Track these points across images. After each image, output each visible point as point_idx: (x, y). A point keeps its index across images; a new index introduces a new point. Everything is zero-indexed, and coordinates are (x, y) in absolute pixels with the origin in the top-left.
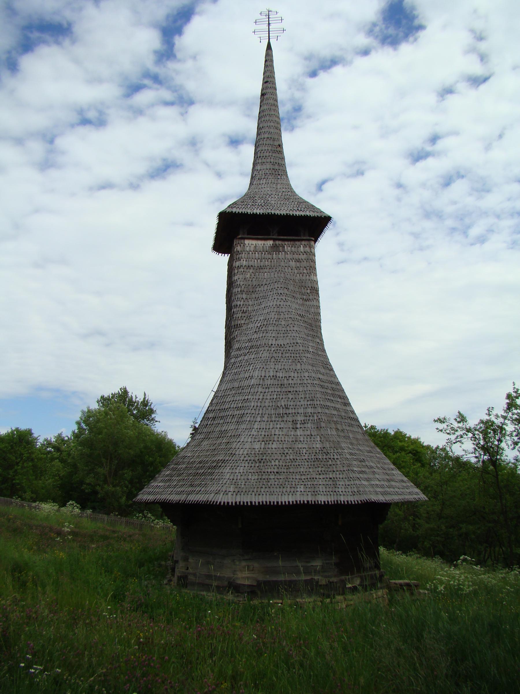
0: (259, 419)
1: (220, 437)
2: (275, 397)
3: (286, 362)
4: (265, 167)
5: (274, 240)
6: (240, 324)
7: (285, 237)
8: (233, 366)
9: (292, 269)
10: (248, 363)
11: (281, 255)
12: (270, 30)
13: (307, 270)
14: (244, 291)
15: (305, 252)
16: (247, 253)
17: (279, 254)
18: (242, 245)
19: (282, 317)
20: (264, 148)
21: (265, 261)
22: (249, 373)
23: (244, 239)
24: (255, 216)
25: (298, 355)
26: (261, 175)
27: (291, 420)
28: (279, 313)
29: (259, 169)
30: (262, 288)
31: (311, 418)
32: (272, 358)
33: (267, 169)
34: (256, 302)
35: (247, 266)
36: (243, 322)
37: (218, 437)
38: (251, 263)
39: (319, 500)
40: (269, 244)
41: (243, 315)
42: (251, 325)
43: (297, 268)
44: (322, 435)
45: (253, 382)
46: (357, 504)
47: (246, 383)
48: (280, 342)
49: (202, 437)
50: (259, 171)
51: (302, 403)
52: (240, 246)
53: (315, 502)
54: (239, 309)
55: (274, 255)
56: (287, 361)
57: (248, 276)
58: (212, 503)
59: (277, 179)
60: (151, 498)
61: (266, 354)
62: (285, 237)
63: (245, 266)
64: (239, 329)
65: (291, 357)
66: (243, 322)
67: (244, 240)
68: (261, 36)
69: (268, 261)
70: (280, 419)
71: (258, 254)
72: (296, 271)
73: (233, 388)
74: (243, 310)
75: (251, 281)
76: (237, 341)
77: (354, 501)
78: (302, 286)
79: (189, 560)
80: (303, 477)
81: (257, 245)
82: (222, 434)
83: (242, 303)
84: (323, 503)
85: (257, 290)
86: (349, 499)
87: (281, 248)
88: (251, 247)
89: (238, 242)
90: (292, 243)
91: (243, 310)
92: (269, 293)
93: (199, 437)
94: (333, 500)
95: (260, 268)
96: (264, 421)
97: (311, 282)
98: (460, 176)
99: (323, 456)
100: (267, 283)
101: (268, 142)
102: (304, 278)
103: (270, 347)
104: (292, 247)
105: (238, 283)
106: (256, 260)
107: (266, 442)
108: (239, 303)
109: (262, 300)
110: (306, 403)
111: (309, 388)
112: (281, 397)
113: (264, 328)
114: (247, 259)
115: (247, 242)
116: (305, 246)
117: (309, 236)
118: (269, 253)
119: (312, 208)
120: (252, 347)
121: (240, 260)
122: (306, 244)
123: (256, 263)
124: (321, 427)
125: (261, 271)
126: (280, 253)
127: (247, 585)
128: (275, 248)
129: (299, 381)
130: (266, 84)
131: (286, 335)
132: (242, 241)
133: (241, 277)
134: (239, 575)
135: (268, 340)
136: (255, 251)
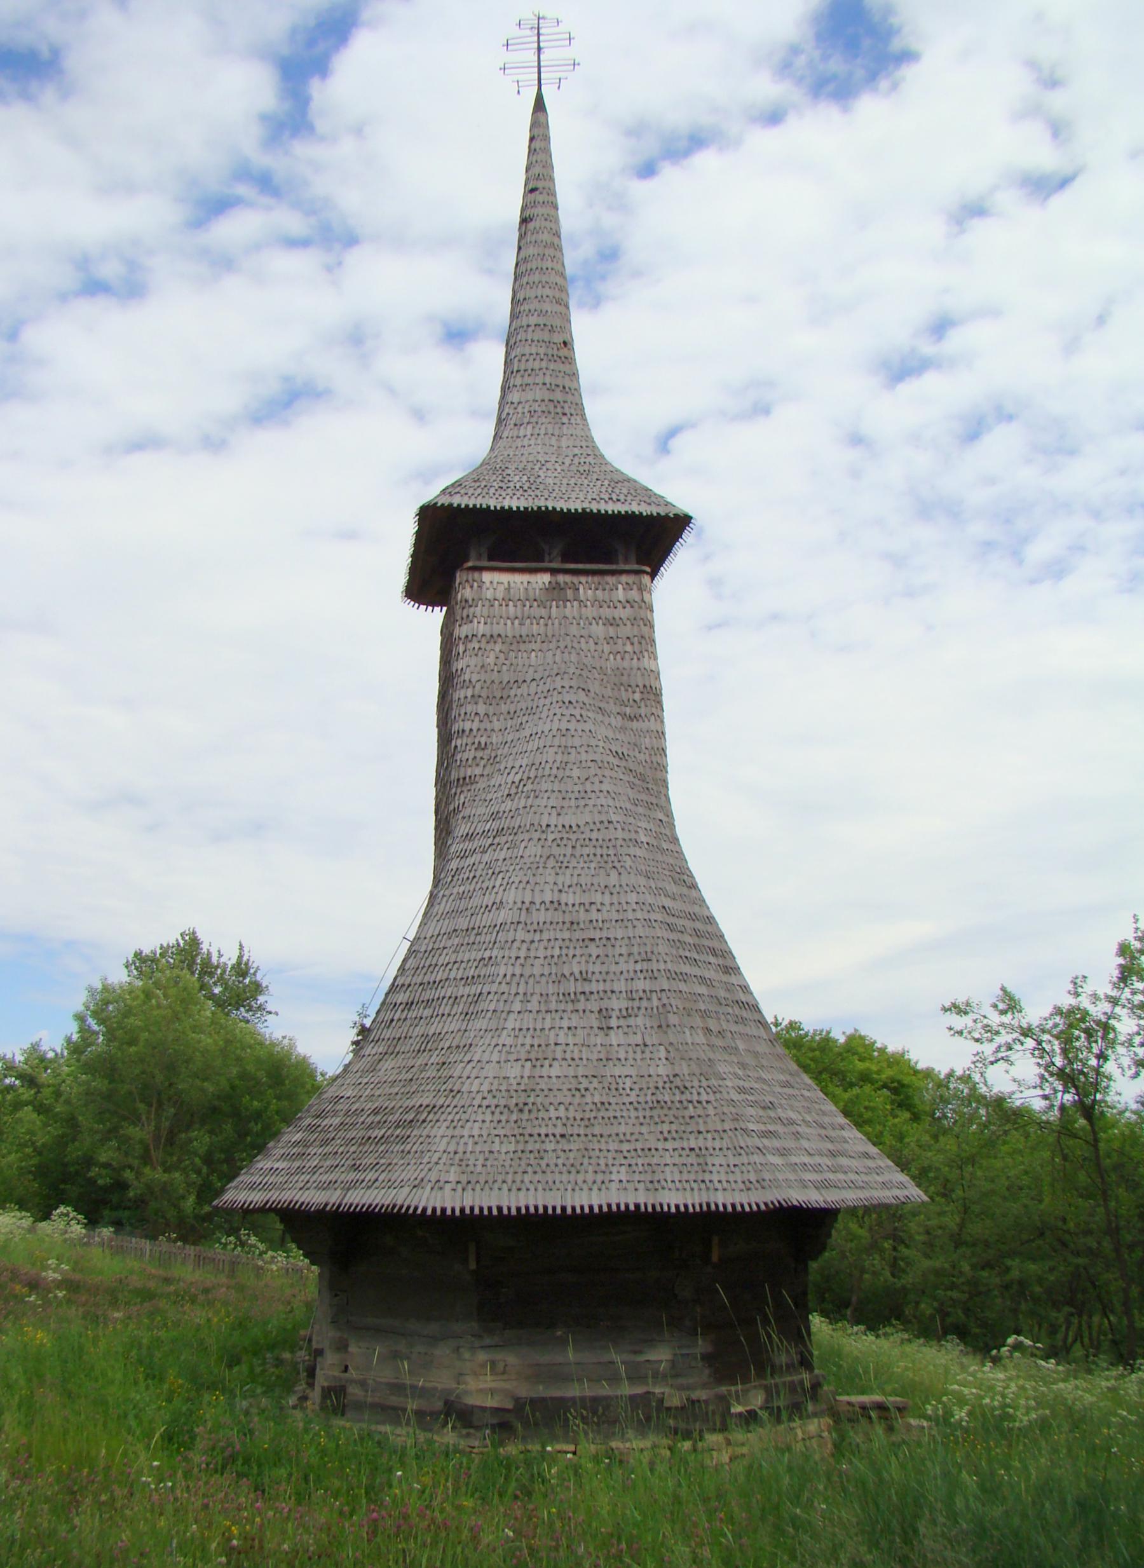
1: (424, 1051)
2: (557, 952)
3: (582, 868)
4: (530, 396)
5: (554, 572)
6: (470, 777)
7: (580, 566)
9: (596, 644)
10: (490, 872)
11: (571, 610)
15: (628, 602)
16: (487, 604)
18: (475, 584)
20: (527, 350)
24: (506, 515)
26: (520, 415)
27: (596, 1009)
28: (565, 749)
30: (524, 689)
32: (548, 857)
36: (478, 771)
37: (419, 1051)
38: (498, 629)
41: (479, 754)
42: (497, 780)
43: (610, 640)
45: (503, 916)
48: (569, 819)
49: (380, 1050)
51: (623, 966)
52: (472, 587)
56: (586, 865)
57: (491, 660)
60: (256, 1198)
61: (534, 850)
62: (580, 566)
64: (469, 787)
68: (520, 78)
74: (479, 743)
76: (464, 818)
79: (350, 1349)
80: (625, 1147)
85: (512, 693)
89: (465, 579)
90: (596, 579)
91: (479, 743)
95: (521, 640)
96: (530, 1011)
99: (674, 1094)
103: (543, 832)
106: (509, 622)
108: (467, 726)
109: (526, 718)
110: (631, 966)
113: (529, 787)
115: (487, 577)
117: (638, 563)
118: (542, 605)
119: (646, 494)
121: (471, 622)
123: (509, 629)
124: (668, 1026)
125: (522, 647)
128: (555, 591)
130: (533, 194)
132: (476, 575)
133: (473, 661)
136: (507, 600)
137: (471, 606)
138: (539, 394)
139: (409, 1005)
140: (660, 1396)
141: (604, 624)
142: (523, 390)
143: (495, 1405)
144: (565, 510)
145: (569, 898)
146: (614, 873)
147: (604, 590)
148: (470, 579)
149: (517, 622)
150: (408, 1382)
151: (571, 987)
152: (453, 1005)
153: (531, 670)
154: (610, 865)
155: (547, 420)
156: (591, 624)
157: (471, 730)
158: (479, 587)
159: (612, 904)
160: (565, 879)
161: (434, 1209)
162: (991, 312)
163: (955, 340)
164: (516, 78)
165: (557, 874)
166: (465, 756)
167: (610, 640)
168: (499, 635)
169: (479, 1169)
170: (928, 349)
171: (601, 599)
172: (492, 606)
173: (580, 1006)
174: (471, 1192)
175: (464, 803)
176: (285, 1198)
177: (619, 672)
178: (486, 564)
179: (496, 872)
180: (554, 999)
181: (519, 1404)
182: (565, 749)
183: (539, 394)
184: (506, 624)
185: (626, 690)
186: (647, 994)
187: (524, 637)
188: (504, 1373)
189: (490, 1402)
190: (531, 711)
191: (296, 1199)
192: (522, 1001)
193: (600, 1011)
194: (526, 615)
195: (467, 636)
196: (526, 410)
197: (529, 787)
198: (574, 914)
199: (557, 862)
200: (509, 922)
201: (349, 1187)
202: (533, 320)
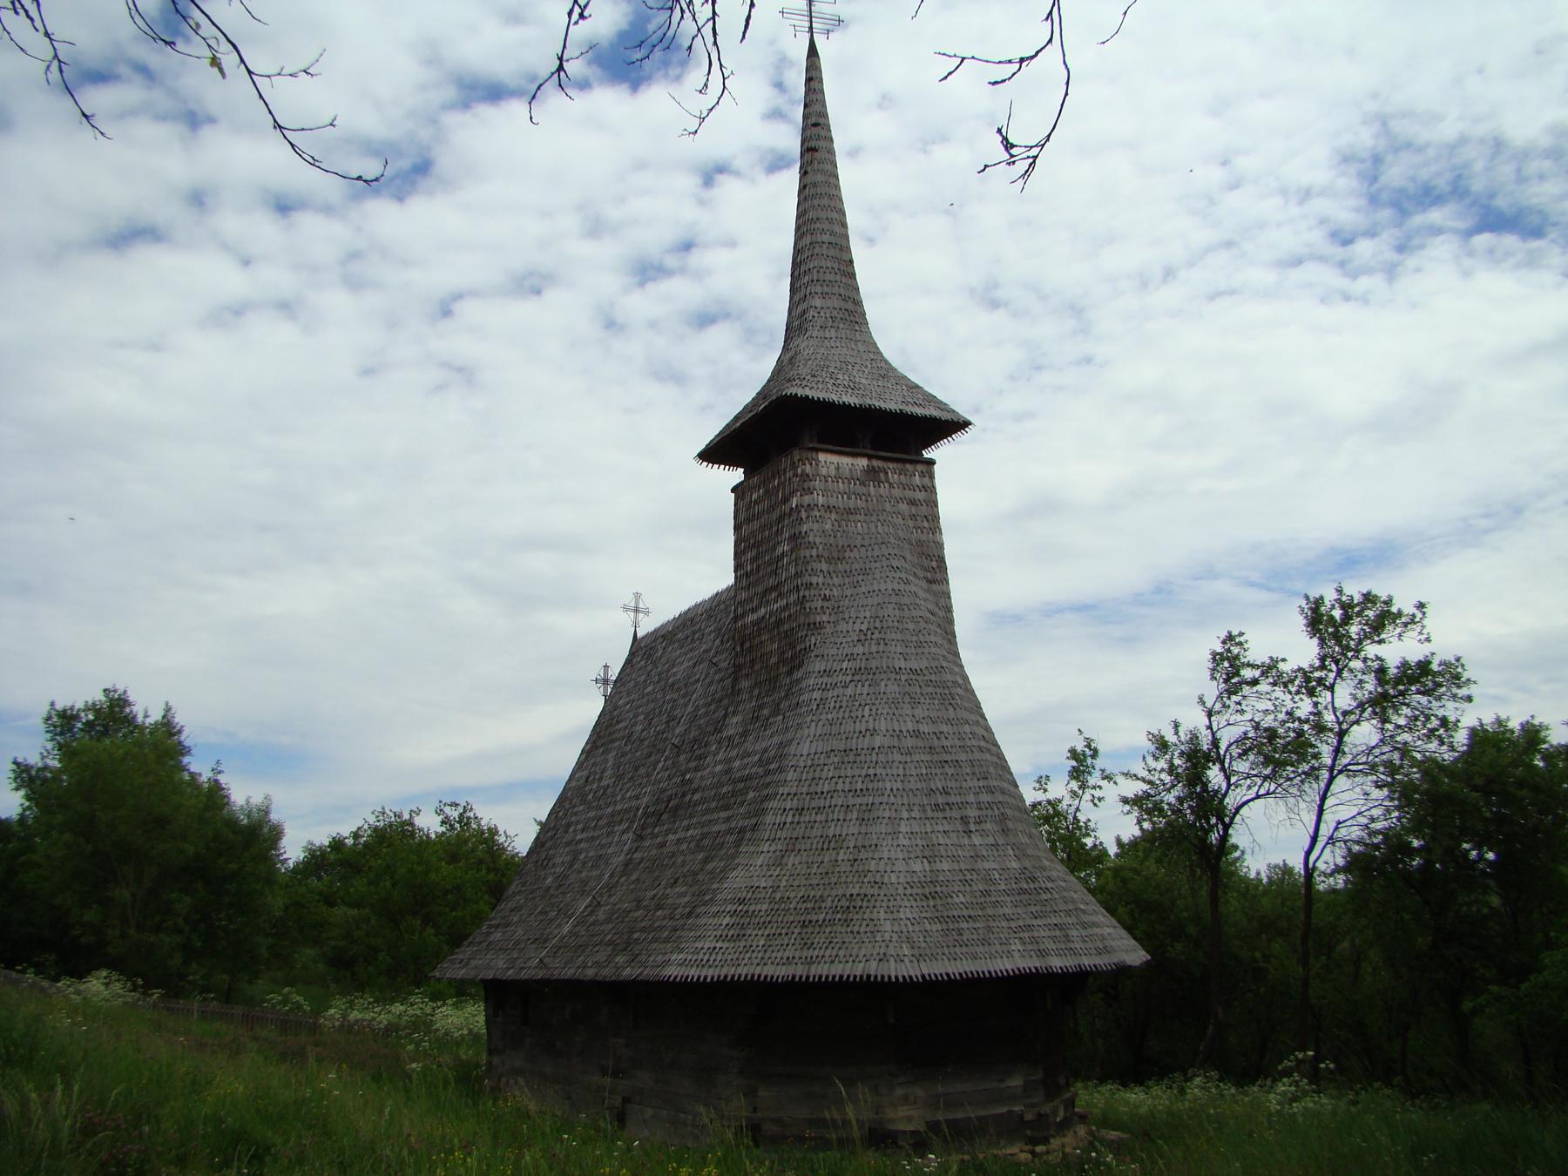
0: (905, 815)
1: (828, 849)
2: (924, 771)
3: (929, 704)
4: (829, 303)
5: (870, 457)
6: (820, 623)
7: (889, 455)
8: (821, 706)
9: (904, 519)
10: (857, 704)
11: (884, 490)
12: (813, 14)
13: (928, 521)
14: (822, 556)
15: (923, 487)
16: (823, 479)
17: (880, 487)
18: (814, 462)
19: (906, 613)
20: (823, 263)
21: (856, 499)
22: (864, 723)
23: (817, 450)
24: (846, 408)
25: (947, 692)
26: (824, 319)
27: (958, 817)
28: (900, 606)
29: (818, 305)
30: (855, 553)
31: (990, 812)
32: (904, 694)
33: (835, 309)
34: (847, 580)
35: (826, 506)
36: (825, 618)
37: (823, 849)
38: (833, 501)
39: (1053, 965)
40: (860, 465)
41: (826, 604)
42: (842, 626)
43: (913, 517)
44: (1014, 844)
45: (878, 741)
46: (976, 979)
47: (865, 742)
48: (914, 665)
49: (780, 847)
50: (819, 310)
51: (970, 784)
52: (811, 464)
53: (960, 974)
54: (816, 592)
55: (872, 488)
56: (931, 702)
57: (828, 526)
58: (736, 978)
59: (853, 332)
60: (461, 973)
61: (893, 688)
62: (889, 455)
63: (822, 506)
64: (819, 631)
65: (936, 694)
66: (825, 618)
67: (817, 453)
68: (797, 23)
69: (861, 499)
70: (940, 815)
71: (843, 483)
72: (911, 523)
73: (832, 751)
74: (825, 595)
75: (835, 537)
76: (817, 656)
77: (930, 975)
78: (923, 553)
79: (760, 1094)
80: (1013, 924)
81: (841, 465)
82: (836, 842)
83: (821, 580)
84: (958, 977)
85: (847, 555)
86: (1097, 963)
87: (882, 475)
88: (830, 469)
89: (805, 456)
90: (900, 466)
91: (825, 595)
92: (873, 565)
93: (772, 849)
94: (825, 973)
95: (849, 511)
96: (915, 818)
97: (937, 547)
98: (727, 316)
99: (936, 886)
100: (866, 543)
101: (832, 252)
102: (924, 537)
103: (897, 673)
104: (900, 474)
105: (811, 539)
106: (840, 496)
107: (931, 859)
108: (814, 580)
109: (860, 578)
110: (976, 783)
111: (977, 755)
112: (934, 772)
113: (876, 635)
114: (825, 493)
115: (822, 457)
116: (922, 475)
117: (872, 449)
118: (863, 484)
119: (931, 399)
120: (858, 671)
121: (812, 493)
122: (924, 471)
123: (840, 502)
124: (1008, 830)
125: (851, 517)
126: (881, 484)
127: (910, 1131)
128: (872, 473)
129: (957, 741)
130: (816, 129)
131: (919, 651)
132: (814, 455)
133: (815, 527)
134: (890, 1113)
135: (891, 659)
136: (837, 478)
137: (811, 480)
138: (836, 302)
139: (800, 811)
140: (1020, 1113)
141: (907, 503)
142: (824, 298)
143: (912, 1128)
144: (816, 399)
145: (924, 728)
146: (951, 708)
147: (906, 475)
148: (809, 456)
149: (845, 496)
150: (973, 1115)
151: (941, 800)
152: (846, 812)
153: (859, 537)
154: (948, 702)
155: (846, 326)
156: (898, 502)
157: (818, 584)
158: (816, 464)
159: (954, 733)
160: (919, 712)
161: (883, 977)
162: (732, 244)
163: (695, 259)
164: (793, 22)
165: (913, 708)
166: (813, 605)
167: (913, 517)
168: (834, 507)
169: (923, 945)
170: (671, 262)
171: (904, 482)
172: (827, 481)
173: (948, 813)
174: (923, 962)
175: (815, 644)
176: (675, 974)
177: (920, 544)
178: (817, 445)
179: (863, 704)
180: (928, 808)
181: (934, 1127)
182: (900, 606)
183: (836, 302)
184: (837, 497)
185: (927, 559)
186: (990, 805)
187: (852, 511)
188: (915, 1102)
189: (910, 1127)
190: (865, 572)
191: (686, 974)
192: (907, 811)
193: (962, 818)
194: (852, 490)
195: (809, 505)
196: (828, 315)
197: (876, 635)
198: (930, 740)
199: (911, 698)
200: (886, 746)
201: (810, 962)
202: (826, 238)
